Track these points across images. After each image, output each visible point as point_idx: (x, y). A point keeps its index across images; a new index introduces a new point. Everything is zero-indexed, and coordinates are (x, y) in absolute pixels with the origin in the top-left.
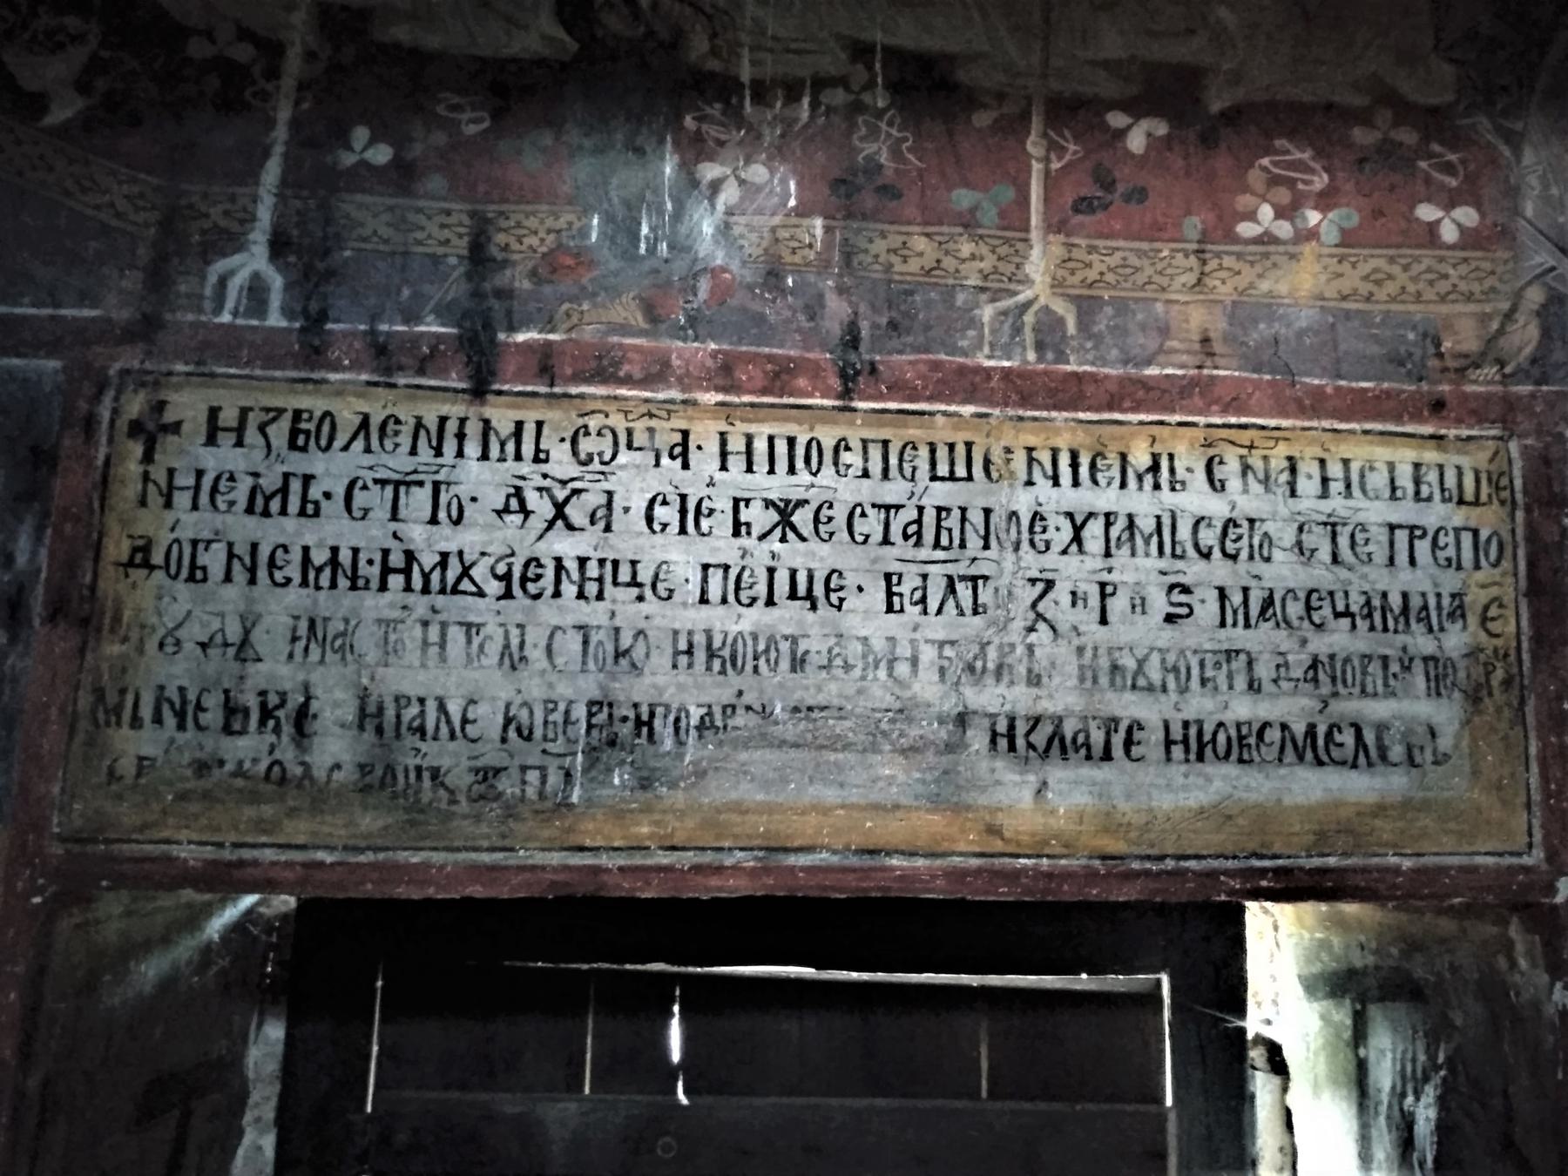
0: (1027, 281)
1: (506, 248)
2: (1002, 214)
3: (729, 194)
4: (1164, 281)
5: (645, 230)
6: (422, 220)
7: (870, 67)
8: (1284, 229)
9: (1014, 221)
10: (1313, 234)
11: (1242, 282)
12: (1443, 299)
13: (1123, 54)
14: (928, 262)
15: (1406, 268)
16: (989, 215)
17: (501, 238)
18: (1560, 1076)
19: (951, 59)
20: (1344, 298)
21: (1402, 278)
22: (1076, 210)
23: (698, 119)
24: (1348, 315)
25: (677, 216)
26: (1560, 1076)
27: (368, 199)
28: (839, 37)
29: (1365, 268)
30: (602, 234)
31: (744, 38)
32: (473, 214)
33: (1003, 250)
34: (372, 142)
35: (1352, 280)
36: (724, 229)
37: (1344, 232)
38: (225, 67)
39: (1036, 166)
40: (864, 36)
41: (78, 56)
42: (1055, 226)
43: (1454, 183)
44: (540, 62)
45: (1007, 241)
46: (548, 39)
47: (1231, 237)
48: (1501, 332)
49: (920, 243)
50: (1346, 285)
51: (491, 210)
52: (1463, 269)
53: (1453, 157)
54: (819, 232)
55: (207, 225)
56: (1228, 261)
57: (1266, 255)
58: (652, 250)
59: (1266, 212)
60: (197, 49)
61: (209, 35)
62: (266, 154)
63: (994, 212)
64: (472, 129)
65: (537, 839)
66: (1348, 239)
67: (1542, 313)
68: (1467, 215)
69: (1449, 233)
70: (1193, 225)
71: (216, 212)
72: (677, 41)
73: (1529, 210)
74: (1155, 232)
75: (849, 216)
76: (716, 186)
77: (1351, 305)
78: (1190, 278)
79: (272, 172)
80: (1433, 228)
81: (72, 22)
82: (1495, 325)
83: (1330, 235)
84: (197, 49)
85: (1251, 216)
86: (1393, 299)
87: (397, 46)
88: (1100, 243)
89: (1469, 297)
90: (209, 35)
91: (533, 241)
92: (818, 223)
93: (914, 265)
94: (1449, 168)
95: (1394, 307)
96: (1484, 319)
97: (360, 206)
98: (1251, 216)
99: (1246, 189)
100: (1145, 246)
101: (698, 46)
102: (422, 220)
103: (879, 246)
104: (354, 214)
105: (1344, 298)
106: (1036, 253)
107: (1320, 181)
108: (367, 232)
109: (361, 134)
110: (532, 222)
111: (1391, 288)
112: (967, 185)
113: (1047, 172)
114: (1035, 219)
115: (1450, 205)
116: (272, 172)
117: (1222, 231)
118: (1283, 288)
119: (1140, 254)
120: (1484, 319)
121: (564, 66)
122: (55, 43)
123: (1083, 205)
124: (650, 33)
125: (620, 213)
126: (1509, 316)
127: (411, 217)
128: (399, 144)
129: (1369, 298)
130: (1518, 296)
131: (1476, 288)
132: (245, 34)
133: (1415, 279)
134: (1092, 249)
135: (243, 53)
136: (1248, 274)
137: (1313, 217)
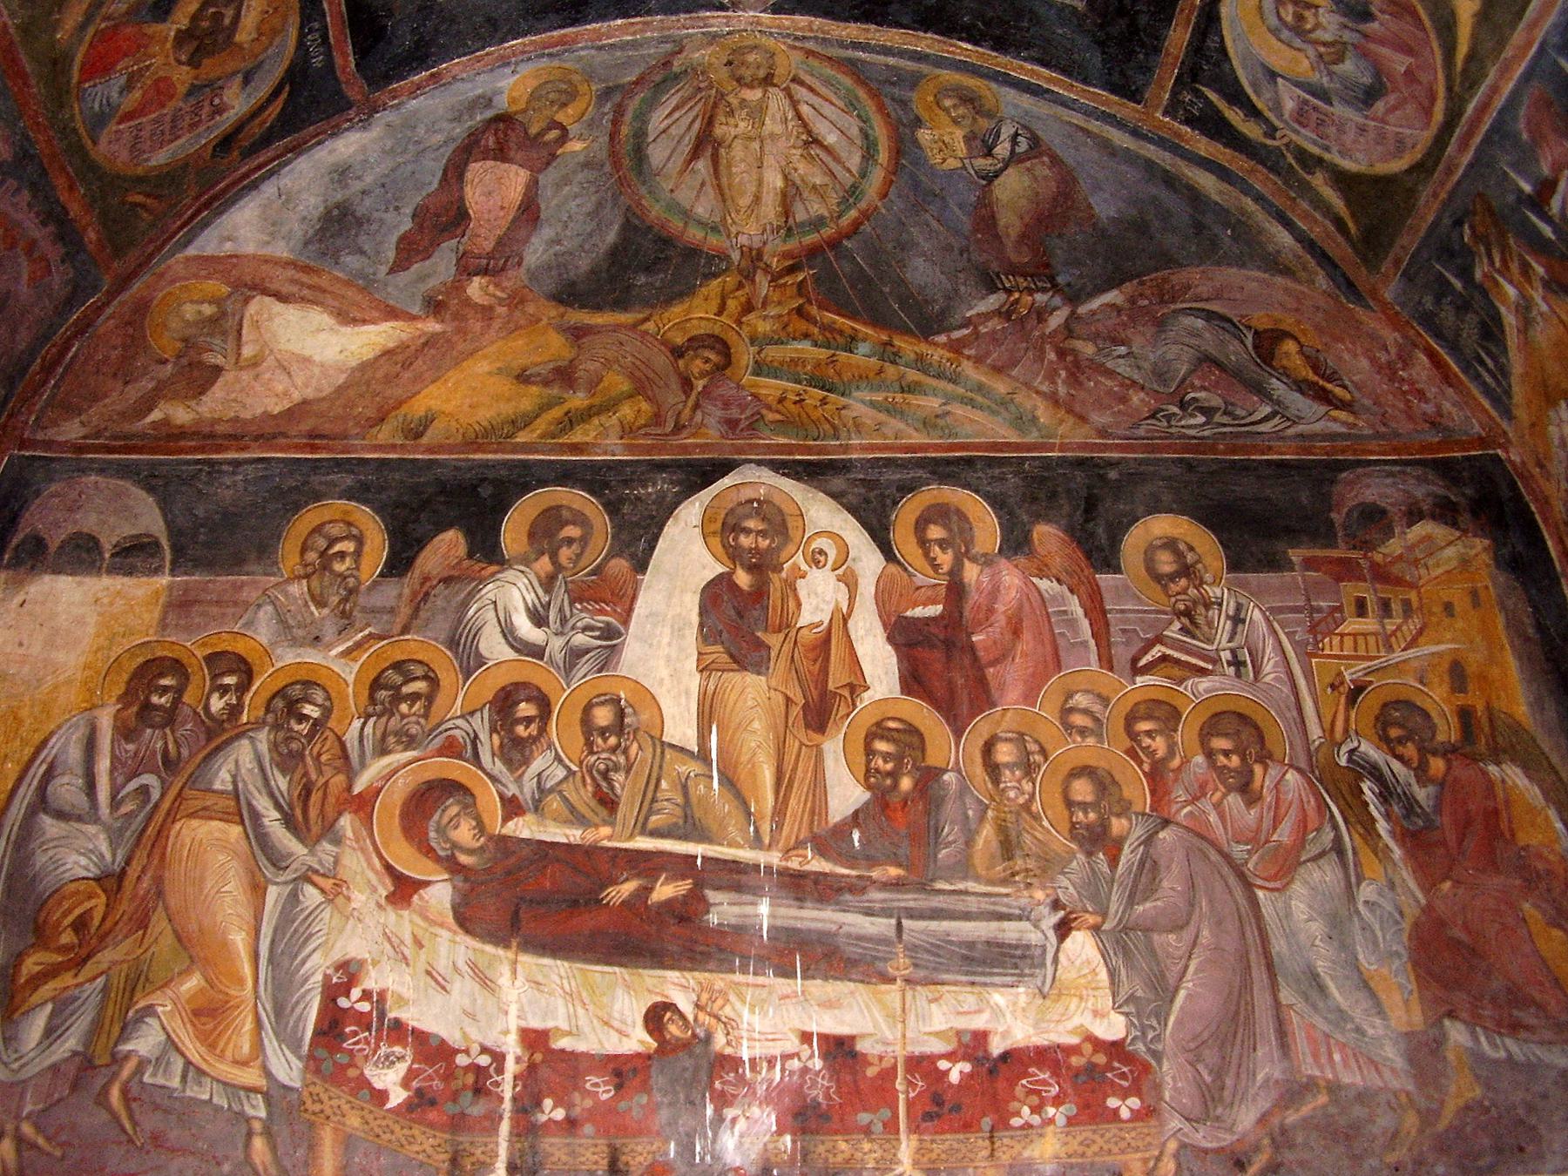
0: (899, 1162)
1: (627, 1164)
2: (885, 1125)
3: (741, 1125)
4: (971, 1156)
5: (698, 1148)
6: (582, 1150)
7: (811, 1045)
8: (1036, 1120)
9: (891, 1126)
10: (1051, 1121)
11: (1015, 1151)
12: (1123, 1152)
13: (944, 1027)
14: (847, 1155)
15: (1102, 1136)
16: (878, 1127)
17: (624, 1158)
18: (856, 835)
19: (852, 1038)
20: (1070, 1156)
21: (1100, 1141)
22: (924, 1120)
23: (723, 1083)
24: (1072, 1166)
25: (714, 1141)
26: (856, 835)
27: (553, 1140)
28: (793, 1030)
29: (1079, 1138)
30: (676, 1152)
31: (745, 1034)
32: (609, 1146)
33: (887, 1146)
34: (555, 1107)
35: (1074, 1145)
36: (740, 1145)
37: (1069, 1118)
38: (478, 1070)
39: (902, 1097)
40: (808, 1029)
41: (402, 1068)
42: (914, 1129)
43: (1125, 1084)
44: (638, 1055)
45: (888, 1141)
46: (642, 1042)
47: (1008, 1127)
48: (1155, 1167)
49: (843, 1145)
50: (1070, 1149)
51: (618, 1142)
52: (1133, 1134)
53: (1125, 1069)
54: (789, 1145)
55: (473, 1159)
56: (1006, 1141)
57: (1026, 1136)
58: (702, 1159)
59: (1026, 1110)
60: (461, 1060)
61: (467, 1052)
62: (501, 1118)
63: (880, 1125)
64: (605, 1097)
65: (285, 435)
66: (1071, 1121)
67: (1176, 1156)
68: (1134, 1102)
69: (1125, 1113)
70: (987, 1122)
71: (478, 1152)
72: (708, 1039)
73: (1167, 1096)
74: (968, 1127)
75: (804, 1131)
76: (734, 1120)
77: (1073, 1160)
78: (985, 1153)
79: (505, 1127)
80: (1116, 1111)
81: (398, 1049)
82: (1151, 1164)
83: (1061, 1121)
84: (461, 1060)
85: (1018, 1114)
86: (1095, 1154)
87: (563, 1051)
88: (937, 1137)
89: (1137, 1150)
90: (467, 1052)
91: (640, 1159)
92: (788, 1138)
93: (840, 1158)
94: (1123, 1076)
95: (1097, 1159)
96: (1145, 1161)
97: (551, 1145)
98: (1018, 1114)
99: (1014, 1098)
100: (961, 1136)
101: (719, 1041)
102: (582, 1150)
103: (821, 1149)
104: (549, 1149)
105: (1070, 1156)
106: (904, 1146)
107: (1055, 1090)
108: (554, 1159)
109: (548, 1103)
110: (639, 1148)
111: (1095, 1148)
112: (865, 1110)
113: (907, 1099)
114: (902, 1126)
115: (1124, 1098)
116: (505, 1127)
117: (1002, 1123)
118: (1036, 1154)
119: (959, 1141)
120: (1145, 1161)
121: (649, 1057)
122: (389, 1061)
123: (928, 1116)
124: (694, 1035)
125: (685, 1139)
126: (1158, 1159)
127: (578, 1149)
128: (569, 1107)
129: (1083, 1155)
130: (1164, 1144)
131: (1140, 1144)
132: (484, 1050)
133: (1108, 1142)
134: (933, 1141)
135: (484, 1060)
136: (1018, 1147)
137: (1051, 1111)
